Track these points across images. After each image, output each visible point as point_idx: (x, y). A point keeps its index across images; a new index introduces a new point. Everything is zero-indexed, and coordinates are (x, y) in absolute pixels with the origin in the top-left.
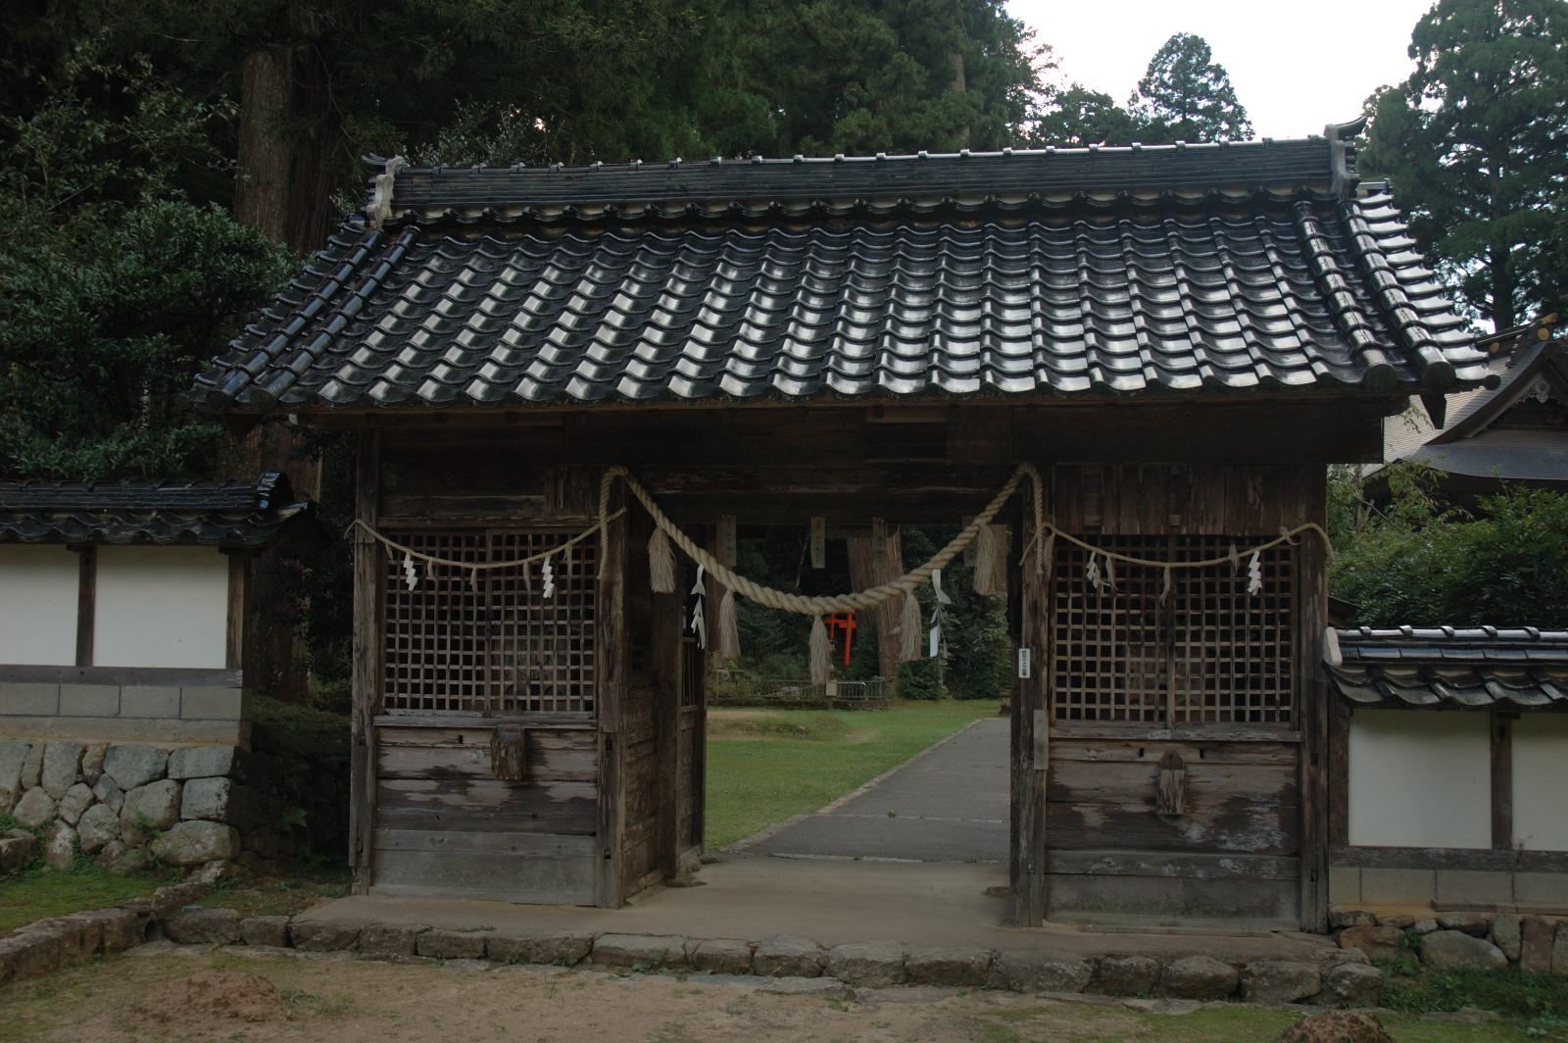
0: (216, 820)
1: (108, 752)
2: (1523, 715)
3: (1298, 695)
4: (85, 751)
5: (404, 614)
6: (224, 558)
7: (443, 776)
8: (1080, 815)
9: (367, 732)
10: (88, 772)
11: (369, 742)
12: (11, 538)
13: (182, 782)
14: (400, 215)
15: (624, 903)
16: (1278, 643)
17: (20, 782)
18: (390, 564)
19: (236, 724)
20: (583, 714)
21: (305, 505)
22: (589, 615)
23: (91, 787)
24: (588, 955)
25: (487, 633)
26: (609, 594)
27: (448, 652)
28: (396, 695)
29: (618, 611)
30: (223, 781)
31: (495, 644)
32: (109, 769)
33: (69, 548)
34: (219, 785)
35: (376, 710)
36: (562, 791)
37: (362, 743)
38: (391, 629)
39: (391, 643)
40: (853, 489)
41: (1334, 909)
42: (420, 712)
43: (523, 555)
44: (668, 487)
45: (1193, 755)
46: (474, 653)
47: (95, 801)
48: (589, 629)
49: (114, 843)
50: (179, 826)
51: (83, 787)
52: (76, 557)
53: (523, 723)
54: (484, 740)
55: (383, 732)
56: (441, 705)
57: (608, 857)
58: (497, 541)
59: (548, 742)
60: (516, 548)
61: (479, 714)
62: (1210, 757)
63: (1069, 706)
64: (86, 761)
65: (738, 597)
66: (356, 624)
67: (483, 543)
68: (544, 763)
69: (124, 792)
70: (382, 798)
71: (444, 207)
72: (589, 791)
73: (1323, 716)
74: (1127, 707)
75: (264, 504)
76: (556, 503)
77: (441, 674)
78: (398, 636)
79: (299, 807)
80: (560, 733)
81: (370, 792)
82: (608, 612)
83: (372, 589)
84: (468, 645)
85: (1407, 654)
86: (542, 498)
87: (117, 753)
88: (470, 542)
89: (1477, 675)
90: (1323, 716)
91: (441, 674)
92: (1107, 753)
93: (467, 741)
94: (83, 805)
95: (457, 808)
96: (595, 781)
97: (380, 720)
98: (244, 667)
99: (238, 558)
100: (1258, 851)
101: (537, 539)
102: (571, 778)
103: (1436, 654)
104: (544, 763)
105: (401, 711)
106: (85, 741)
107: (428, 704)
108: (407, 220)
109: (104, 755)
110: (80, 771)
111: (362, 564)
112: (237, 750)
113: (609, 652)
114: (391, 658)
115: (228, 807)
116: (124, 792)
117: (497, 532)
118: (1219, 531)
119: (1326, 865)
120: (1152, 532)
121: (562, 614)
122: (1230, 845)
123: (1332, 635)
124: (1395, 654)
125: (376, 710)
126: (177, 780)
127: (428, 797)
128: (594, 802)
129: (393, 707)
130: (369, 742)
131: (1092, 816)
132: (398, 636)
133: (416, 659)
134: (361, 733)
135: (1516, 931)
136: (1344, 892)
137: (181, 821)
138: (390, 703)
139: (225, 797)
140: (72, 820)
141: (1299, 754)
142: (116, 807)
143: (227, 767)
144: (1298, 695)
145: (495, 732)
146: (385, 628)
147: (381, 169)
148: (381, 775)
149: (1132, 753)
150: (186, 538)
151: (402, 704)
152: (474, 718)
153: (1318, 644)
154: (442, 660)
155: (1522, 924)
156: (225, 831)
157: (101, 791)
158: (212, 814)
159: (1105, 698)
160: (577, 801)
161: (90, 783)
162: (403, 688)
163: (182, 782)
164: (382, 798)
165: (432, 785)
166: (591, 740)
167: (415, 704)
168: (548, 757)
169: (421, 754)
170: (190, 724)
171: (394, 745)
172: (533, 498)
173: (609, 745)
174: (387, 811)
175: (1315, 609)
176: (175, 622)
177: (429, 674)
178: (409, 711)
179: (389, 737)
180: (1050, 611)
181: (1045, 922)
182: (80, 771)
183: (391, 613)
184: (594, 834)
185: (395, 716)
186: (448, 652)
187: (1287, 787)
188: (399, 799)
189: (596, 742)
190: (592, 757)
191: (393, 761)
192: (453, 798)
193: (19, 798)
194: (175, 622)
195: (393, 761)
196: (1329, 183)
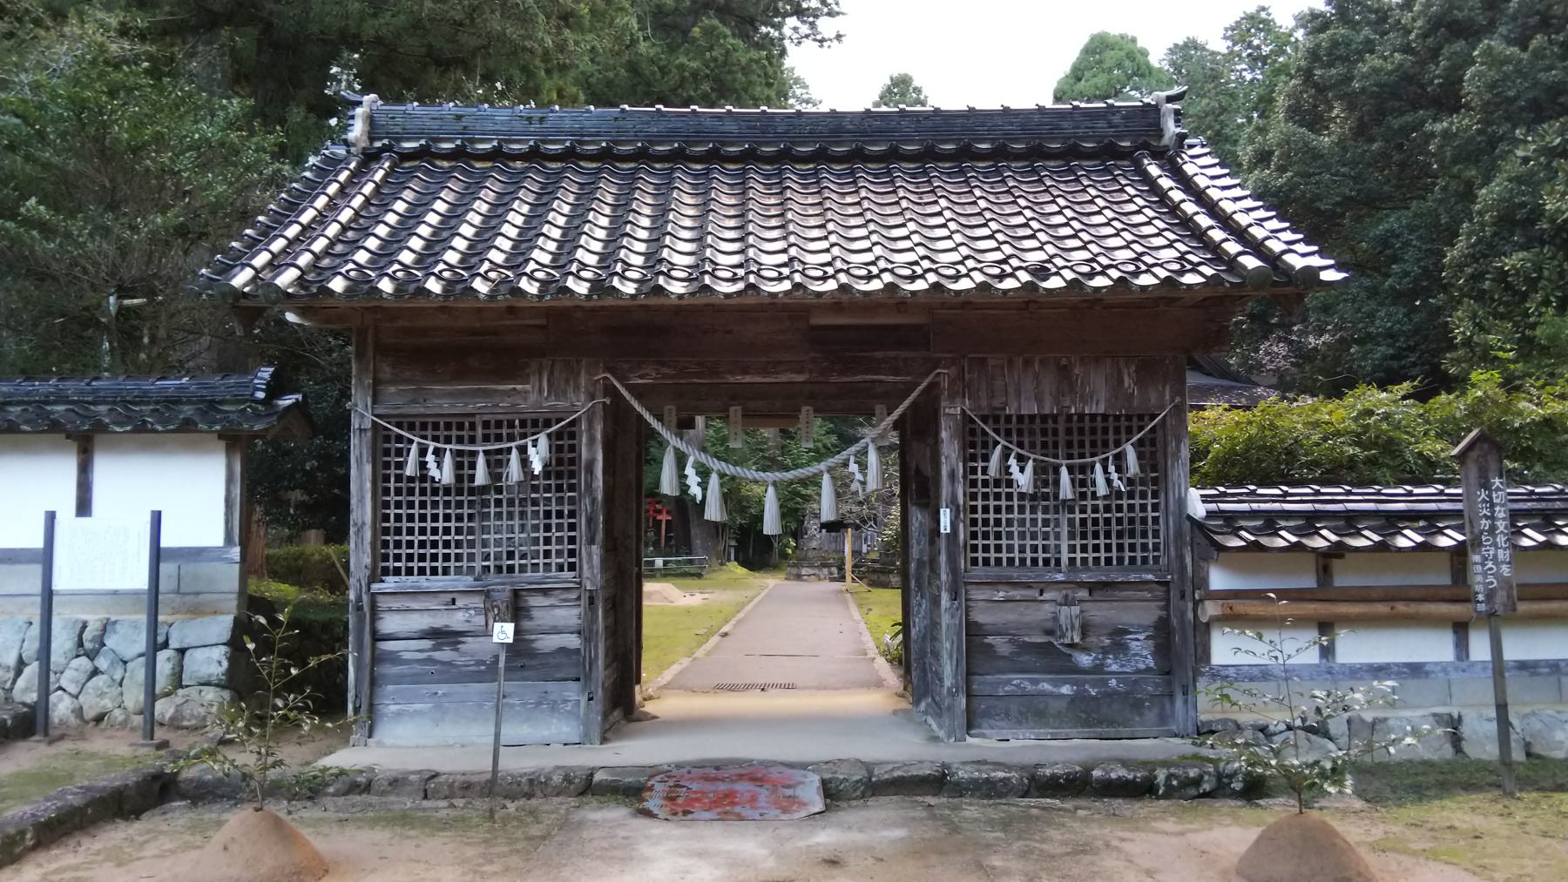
0: (217, 685)
1: (106, 627)
2: (1348, 555)
3: (1167, 544)
4: (85, 626)
5: (398, 492)
6: (222, 444)
7: (441, 636)
8: (990, 646)
9: (365, 597)
10: (88, 645)
11: (366, 609)
12: (12, 428)
13: (182, 652)
14: (378, 144)
15: (604, 740)
16: (1150, 501)
17: (20, 657)
18: (395, 447)
19: (234, 596)
20: (567, 574)
21: (300, 397)
22: (572, 488)
23: (92, 660)
24: (408, 610)
25: (478, 507)
26: (590, 469)
27: (440, 524)
28: (391, 564)
29: (599, 482)
30: (224, 649)
31: (486, 516)
32: (110, 642)
33: (68, 437)
34: (220, 653)
35: (373, 578)
36: (548, 643)
37: (359, 609)
38: (386, 505)
39: (386, 518)
40: (800, 378)
41: (1203, 717)
42: (415, 578)
43: (511, 438)
44: (641, 377)
45: (1083, 594)
46: (465, 524)
47: (96, 672)
48: (572, 501)
49: (117, 712)
50: (181, 692)
51: (84, 660)
52: (74, 447)
53: (513, 584)
54: (478, 601)
55: (380, 598)
56: (434, 571)
57: (590, 699)
58: (486, 425)
59: (535, 601)
60: (504, 431)
61: (470, 579)
62: (1097, 595)
63: (980, 555)
64: (87, 635)
65: (722, 475)
66: (353, 501)
67: (473, 426)
68: (531, 618)
69: (125, 663)
70: (377, 659)
71: (418, 139)
72: (573, 641)
73: (1188, 560)
74: (1004, 555)
75: (261, 395)
76: (541, 391)
77: (434, 544)
78: (392, 512)
79: (298, 662)
80: (545, 592)
81: (368, 653)
82: (589, 486)
83: (368, 468)
84: (459, 518)
85: (1255, 506)
86: (528, 387)
87: (118, 627)
88: (460, 427)
89: (1270, 522)
90: (1188, 560)
91: (434, 544)
92: (1016, 594)
93: (459, 603)
94: (83, 678)
95: (450, 663)
96: (579, 633)
97: (375, 587)
98: (241, 544)
99: (232, 441)
100: (1138, 671)
101: (523, 424)
102: (556, 631)
103: (1277, 506)
104: (531, 618)
105: (396, 578)
106: (85, 617)
107: (422, 571)
108: (385, 149)
109: (104, 630)
110: (80, 644)
111: (359, 449)
112: (236, 619)
113: (590, 521)
114: (386, 531)
115: (230, 672)
116: (125, 663)
117: (486, 418)
118: (1101, 410)
119: (1195, 681)
120: (1047, 411)
121: (548, 489)
122: (1114, 668)
123: (1194, 494)
124: (1244, 507)
125: (373, 578)
126: (177, 650)
127: (424, 655)
128: (578, 650)
129: (388, 574)
130: (366, 609)
131: (1001, 644)
132: (392, 512)
133: (410, 531)
134: (359, 599)
135: (1345, 727)
136: (1207, 705)
137: (182, 687)
138: (386, 572)
139: (225, 664)
140: (73, 689)
141: (1168, 592)
142: (118, 677)
143: (226, 636)
144: (1167, 544)
145: (487, 594)
146: (380, 506)
147: (359, 103)
148: (377, 637)
149: (1034, 593)
150: (187, 426)
151: (397, 572)
152: (466, 581)
153: (1182, 503)
154: (435, 531)
155: (1349, 721)
156: (227, 694)
157: (102, 663)
158: (214, 679)
159: (986, 549)
160: (563, 650)
161: (92, 655)
162: (398, 558)
163: (182, 652)
164: (377, 659)
165: (427, 644)
166: (574, 596)
167: (410, 572)
168: (535, 613)
169: (416, 616)
170: (188, 598)
171: (390, 610)
172: (519, 387)
173: (592, 601)
174: (388, 669)
175: (1179, 471)
176: (183, 497)
177: (422, 544)
178: (404, 578)
179: (383, 603)
180: (965, 477)
181: (969, 740)
182: (80, 644)
183: (386, 491)
184: (578, 679)
185: (390, 583)
186: (440, 524)
187: (1160, 618)
188: (394, 658)
189: (579, 598)
190: (576, 611)
191: (389, 624)
192: (445, 655)
193: (19, 672)
194: (183, 497)
195: (389, 624)
196: (1161, 136)
